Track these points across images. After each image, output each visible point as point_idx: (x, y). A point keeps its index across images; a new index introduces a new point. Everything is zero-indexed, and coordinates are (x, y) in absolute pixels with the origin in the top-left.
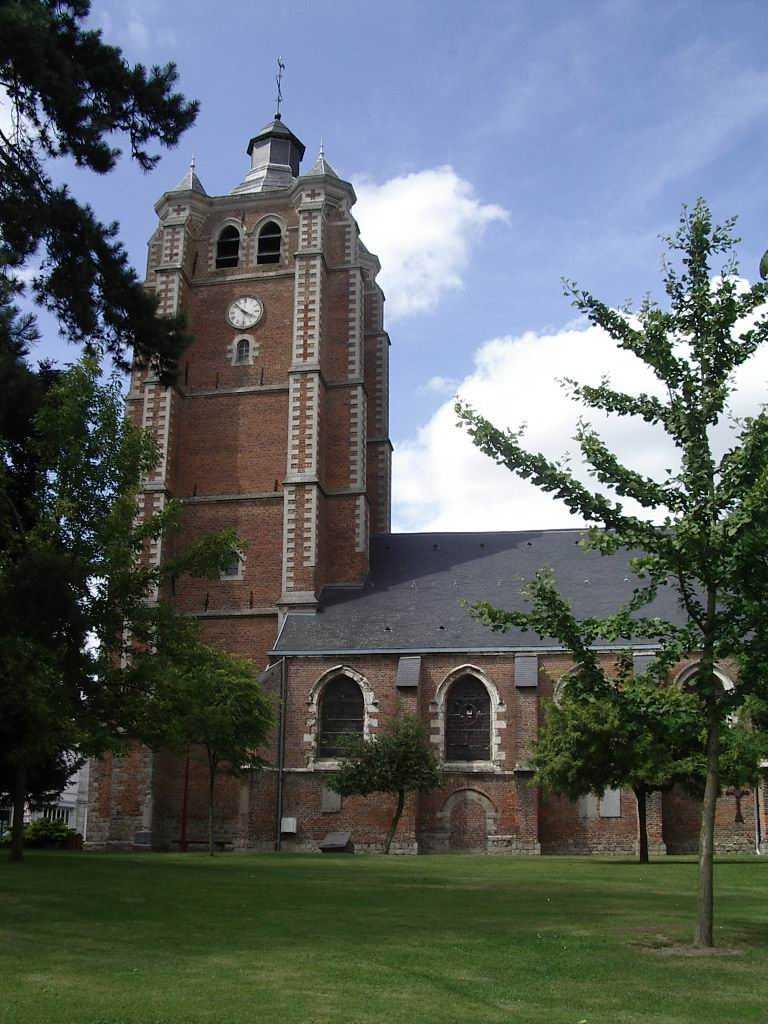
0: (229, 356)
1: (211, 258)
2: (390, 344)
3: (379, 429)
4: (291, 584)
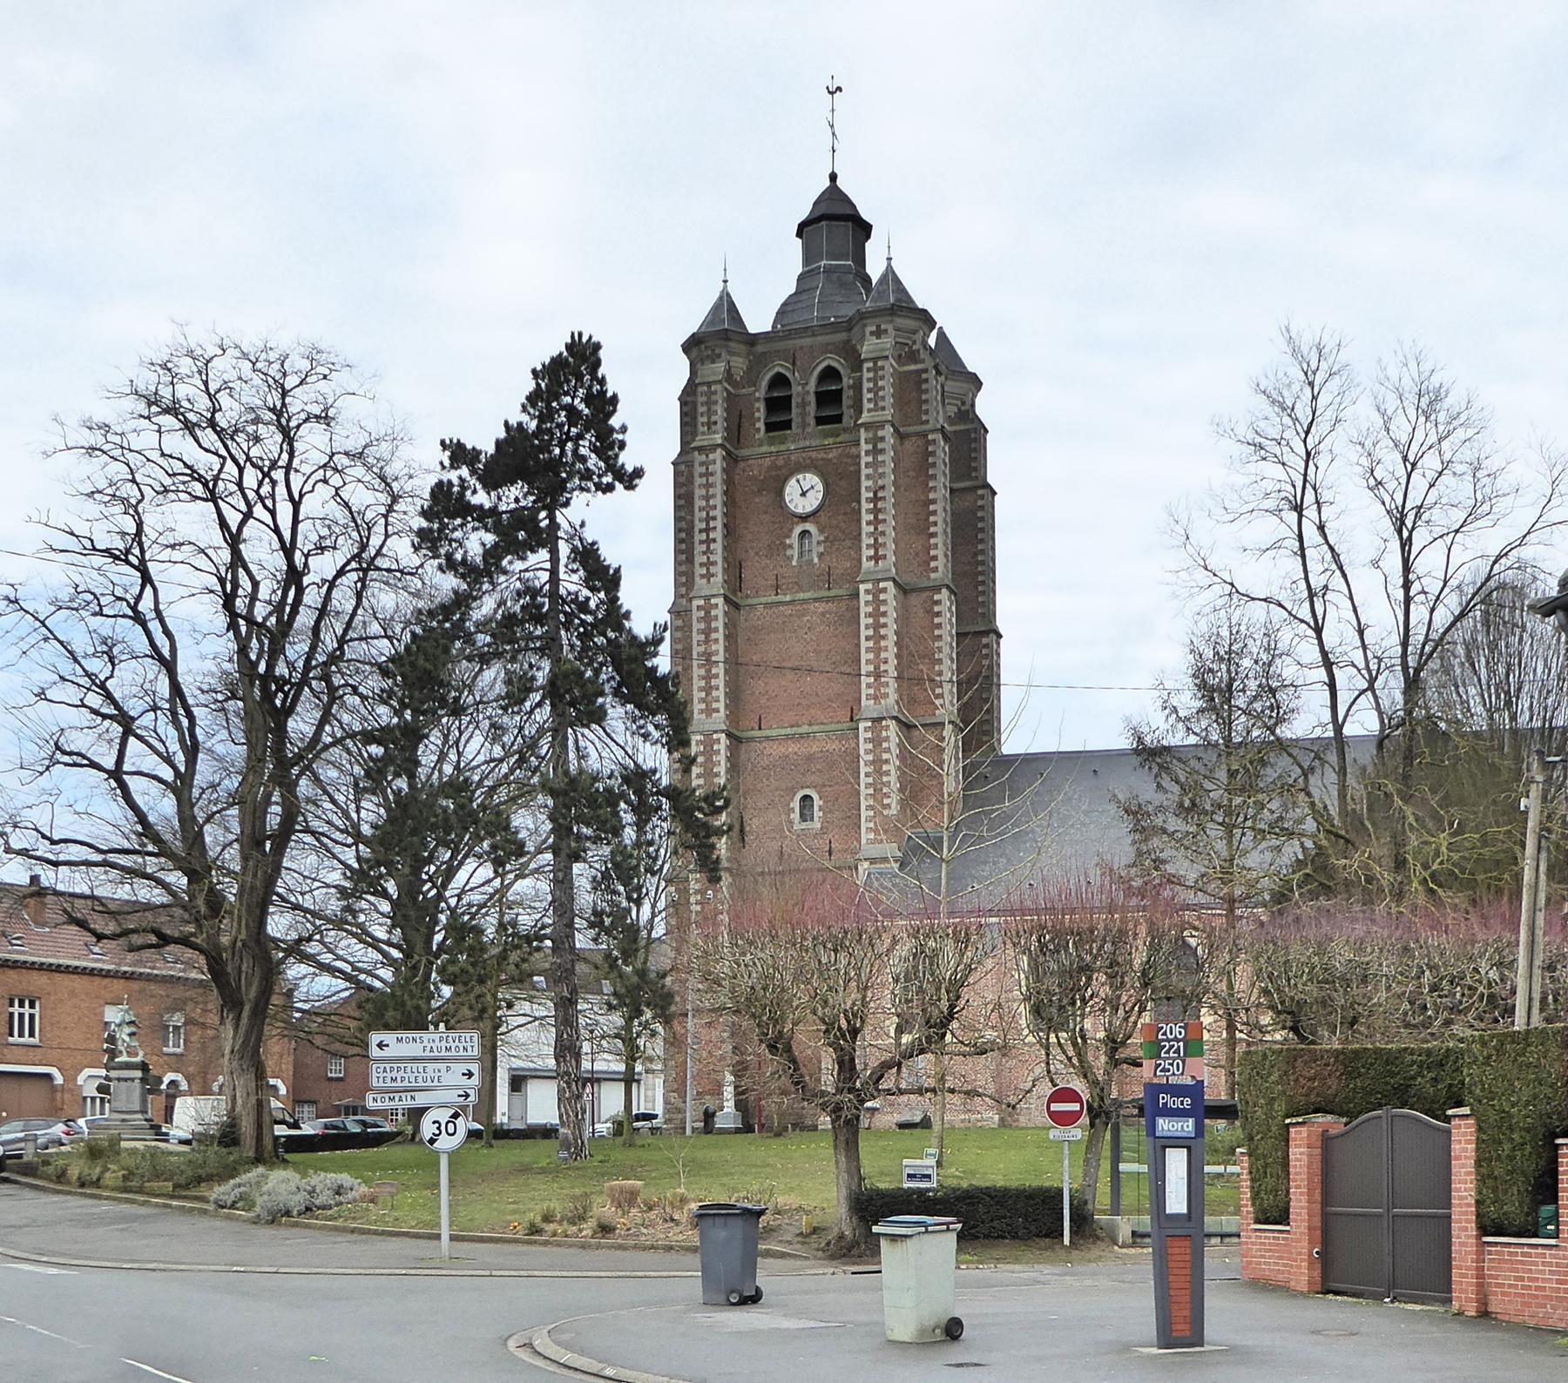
0: (789, 552)
1: (759, 419)
2: (994, 493)
4: (872, 836)
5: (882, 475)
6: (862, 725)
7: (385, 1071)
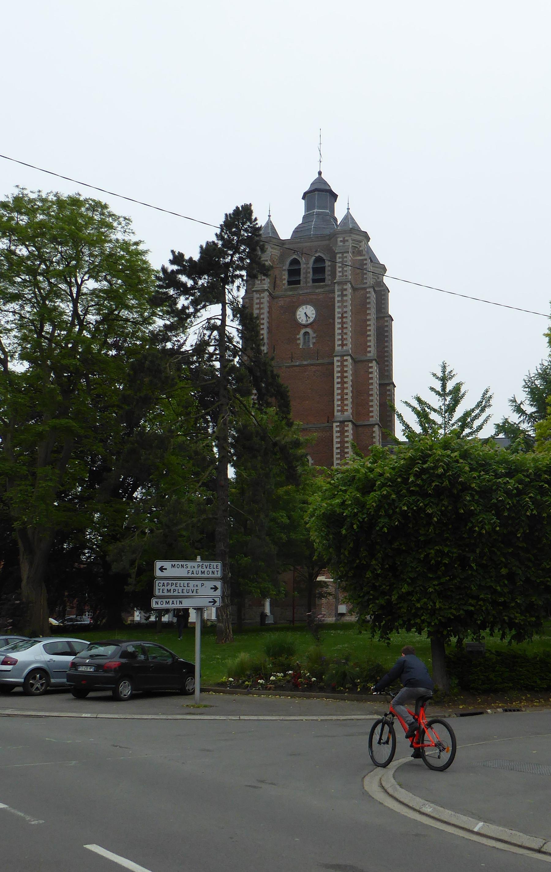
0: (298, 342)
1: (285, 279)
2: (392, 320)
3: (388, 375)
5: (346, 307)
6: (335, 425)
7: (163, 585)
